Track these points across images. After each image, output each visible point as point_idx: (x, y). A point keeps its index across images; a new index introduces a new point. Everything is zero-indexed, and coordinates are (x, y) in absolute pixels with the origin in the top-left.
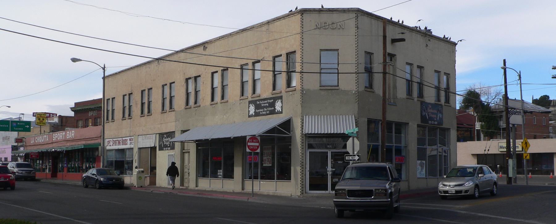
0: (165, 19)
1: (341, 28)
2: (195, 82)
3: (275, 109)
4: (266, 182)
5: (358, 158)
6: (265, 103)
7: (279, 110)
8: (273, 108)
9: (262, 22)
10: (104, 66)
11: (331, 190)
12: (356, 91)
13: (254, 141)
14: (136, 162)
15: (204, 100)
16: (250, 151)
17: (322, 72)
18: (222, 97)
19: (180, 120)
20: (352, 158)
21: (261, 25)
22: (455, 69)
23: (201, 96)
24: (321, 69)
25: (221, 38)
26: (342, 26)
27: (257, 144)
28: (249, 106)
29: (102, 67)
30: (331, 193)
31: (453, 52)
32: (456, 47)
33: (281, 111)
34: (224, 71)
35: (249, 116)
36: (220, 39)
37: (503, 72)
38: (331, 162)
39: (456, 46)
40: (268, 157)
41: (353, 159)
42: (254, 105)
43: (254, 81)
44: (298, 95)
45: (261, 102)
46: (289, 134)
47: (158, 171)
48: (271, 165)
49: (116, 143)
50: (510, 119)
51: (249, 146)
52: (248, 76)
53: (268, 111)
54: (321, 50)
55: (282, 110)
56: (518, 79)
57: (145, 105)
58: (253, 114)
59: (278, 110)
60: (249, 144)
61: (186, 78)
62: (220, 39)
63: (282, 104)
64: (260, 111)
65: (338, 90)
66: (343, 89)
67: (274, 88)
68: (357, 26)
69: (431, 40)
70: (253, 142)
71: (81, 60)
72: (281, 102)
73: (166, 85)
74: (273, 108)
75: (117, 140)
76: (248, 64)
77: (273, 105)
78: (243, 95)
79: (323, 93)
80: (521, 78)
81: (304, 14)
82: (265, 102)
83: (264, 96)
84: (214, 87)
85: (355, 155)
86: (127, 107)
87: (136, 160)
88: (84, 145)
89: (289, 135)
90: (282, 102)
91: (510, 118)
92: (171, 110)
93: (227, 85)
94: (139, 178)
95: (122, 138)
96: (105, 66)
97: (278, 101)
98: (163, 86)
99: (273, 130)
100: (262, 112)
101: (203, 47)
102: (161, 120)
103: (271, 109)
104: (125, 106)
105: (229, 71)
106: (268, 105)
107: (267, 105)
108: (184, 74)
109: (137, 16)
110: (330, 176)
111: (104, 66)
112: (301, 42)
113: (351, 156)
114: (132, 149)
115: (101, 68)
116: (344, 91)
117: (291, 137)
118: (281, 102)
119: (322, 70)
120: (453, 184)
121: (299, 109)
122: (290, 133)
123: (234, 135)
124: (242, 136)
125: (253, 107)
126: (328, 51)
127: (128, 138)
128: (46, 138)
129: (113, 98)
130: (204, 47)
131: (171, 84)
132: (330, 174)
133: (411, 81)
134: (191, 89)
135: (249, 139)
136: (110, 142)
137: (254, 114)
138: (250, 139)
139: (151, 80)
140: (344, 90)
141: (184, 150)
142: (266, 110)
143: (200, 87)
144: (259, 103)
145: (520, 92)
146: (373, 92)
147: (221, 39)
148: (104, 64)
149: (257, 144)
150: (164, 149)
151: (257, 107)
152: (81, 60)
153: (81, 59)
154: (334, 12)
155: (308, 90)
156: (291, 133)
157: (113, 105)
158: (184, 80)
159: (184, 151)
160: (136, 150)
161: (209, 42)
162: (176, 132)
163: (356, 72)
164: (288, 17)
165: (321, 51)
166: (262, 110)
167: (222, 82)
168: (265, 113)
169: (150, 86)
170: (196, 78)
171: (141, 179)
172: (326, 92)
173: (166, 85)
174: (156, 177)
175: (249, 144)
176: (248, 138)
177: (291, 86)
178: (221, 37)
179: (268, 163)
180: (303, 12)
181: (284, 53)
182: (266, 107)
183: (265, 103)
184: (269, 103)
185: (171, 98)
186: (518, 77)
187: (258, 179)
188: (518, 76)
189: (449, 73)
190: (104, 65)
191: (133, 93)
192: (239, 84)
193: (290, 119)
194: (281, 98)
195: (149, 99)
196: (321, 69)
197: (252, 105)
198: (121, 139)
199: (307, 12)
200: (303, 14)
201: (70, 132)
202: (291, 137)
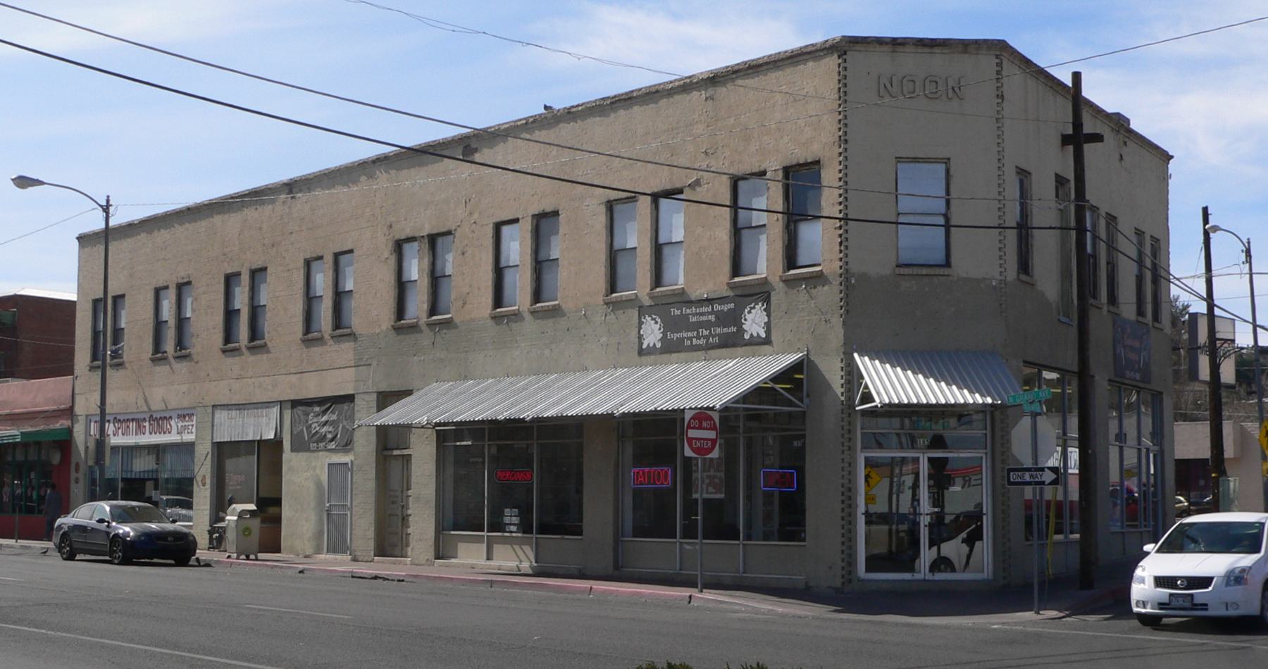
0: (528, 44)
1: (956, 91)
2: (429, 253)
3: (741, 331)
5: (1055, 476)
6: (702, 314)
7: (755, 335)
8: (733, 329)
9: (690, 77)
10: (108, 201)
12: (1001, 280)
13: (704, 424)
15: (464, 304)
16: (692, 454)
17: (900, 221)
19: (375, 363)
20: (1031, 476)
21: (688, 86)
22: (1168, 227)
23: (452, 292)
24: (899, 214)
26: (957, 90)
27: (711, 435)
28: (640, 323)
29: (101, 203)
30: (930, 579)
31: (1164, 178)
32: (1169, 166)
33: (763, 335)
34: (542, 218)
35: (641, 352)
37: (1202, 241)
38: (929, 487)
39: (1168, 163)
40: (712, 473)
41: (1036, 480)
42: (659, 321)
43: (658, 250)
44: (830, 295)
45: (689, 311)
46: (800, 404)
47: (287, 511)
48: (722, 496)
50: (1222, 366)
51: (690, 440)
52: (634, 236)
53: (714, 337)
54: (899, 159)
55: (768, 332)
56: (1244, 260)
58: (654, 344)
59: (752, 335)
60: (693, 433)
61: (396, 238)
63: (769, 315)
64: (685, 335)
67: (736, 270)
68: (1000, 93)
69: (1128, 143)
70: (700, 428)
71: (42, 183)
72: (765, 310)
73: (166, 288)
74: (733, 329)
77: (735, 318)
80: (1250, 256)
81: (848, 53)
82: (704, 309)
83: (697, 293)
86: (172, 323)
87: (204, 477)
89: (799, 407)
90: (768, 310)
91: (1220, 365)
94: (244, 532)
96: (111, 203)
97: (754, 308)
98: (308, 263)
99: (758, 393)
100: (690, 339)
102: (302, 361)
103: (725, 330)
105: (561, 217)
106: (713, 320)
107: (712, 318)
108: (391, 226)
109: (453, 31)
111: (108, 201)
112: (841, 133)
113: (1029, 470)
114: (189, 447)
115: (97, 206)
118: (765, 310)
119: (900, 215)
121: (836, 334)
122: (802, 403)
125: (658, 326)
126: (919, 162)
131: (337, 256)
132: (927, 523)
133: (1092, 256)
135: (691, 419)
136: (190, 427)
137: (659, 345)
138: (693, 418)
139: (264, 245)
142: (706, 333)
143: (450, 263)
144: (678, 312)
145: (1256, 293)
146: (1033, 285)
148: (108, 197)
149: (711, 435)
150: (313, 446)
151: (670, 325)
152: (42, 183)
153: (40, 179)
154: (936, 50)
156: (806, 400)
158: (390, 245)
160: (204, 451)
163: (1000, 224)
165: (898, 162)
166: (690, 334)
167: (536, 251)
168: (702, 341)
169: (260, 263)
170: (433, 239)
171: (250, 534)
172: (914, 282)
173: (166, 288)
174: (280, 528)
175: (693, 433)
176: (688, 416)
177: (313, 331)
178: (531, 120)
179: (711, 489)
180: (846, 47)
181: (774, 165)
182: (707, 325)
183: (702, 314)
184: (718, 315)
186: (1244, 254)
188: (1242, 251)
189: (1159, 238)
190: (106, 198)
191: (193, 282)
192: (602, 257)
193: (803, 360)
194: (766, 298)
196: (899, 214)
197: (653, 319)
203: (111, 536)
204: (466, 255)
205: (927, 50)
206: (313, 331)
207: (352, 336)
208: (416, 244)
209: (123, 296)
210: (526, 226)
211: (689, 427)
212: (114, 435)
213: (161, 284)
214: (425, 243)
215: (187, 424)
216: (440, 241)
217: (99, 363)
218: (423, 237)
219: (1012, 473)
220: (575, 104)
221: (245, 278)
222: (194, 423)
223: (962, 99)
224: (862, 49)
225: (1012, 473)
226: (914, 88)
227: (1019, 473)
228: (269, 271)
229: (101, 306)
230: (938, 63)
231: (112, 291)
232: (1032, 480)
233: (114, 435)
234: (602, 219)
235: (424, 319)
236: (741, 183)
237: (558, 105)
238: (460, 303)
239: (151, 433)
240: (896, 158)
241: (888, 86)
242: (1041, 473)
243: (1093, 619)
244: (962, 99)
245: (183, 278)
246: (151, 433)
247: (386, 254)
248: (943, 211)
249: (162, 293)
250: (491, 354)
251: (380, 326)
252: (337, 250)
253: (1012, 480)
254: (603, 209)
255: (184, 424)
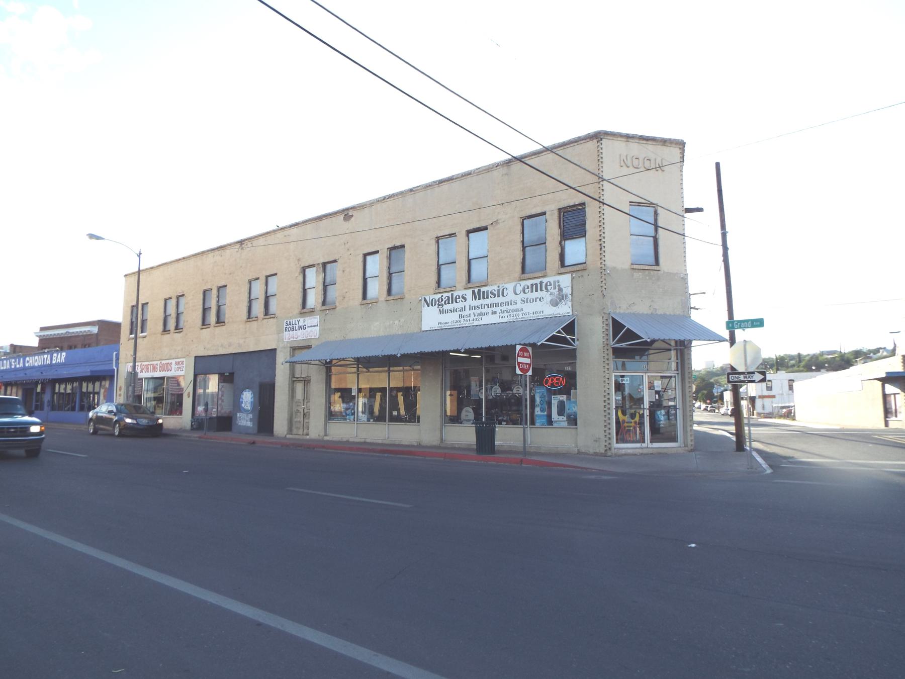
4: (500, 428)
5: (763, 377)
11: (651, 442)
14: (189, 397)
18: (388, 291)
25: (388, 199)
36: (384, 199)
41: (749, 379)
43: (267, 299)
49: (148, 368)
57: (147, 322)
60: (520, 360)
62: (384, 199)
65: (659, 272)
66: (666, 271)
70: (523, 356)
73: (170, 298)
75: (151, 365)
76: (455, 234)
78: (439, 287)
79: (637, 275)
81: (603, 139)
84: (366, 277)
85: (753, 373)
86: (174, 315)
88: (91, 372)
92: (266, 317)
93: (404, 271)
95: (140, 362)
98: (166, 300)
101: (343, 215)
104: (167, 314)
110: (648, 417)
116: (669, 274)
117: (575, 350)
120: (196, 435)
123: (464, 345)
124: (432, 352)
127: (173, 361)
128: (47, 358)
129: (221, 288)
130: (345, 215)
134: (172, 310)
139: (225, 274)
140: (668, 273)
141: (295, 377)
147: (386, 200)
154: (649, 142)
155: (615, 268)
157: (143, 314)
158: (299, 270)
159: (294, 379)
161: (358, 207)
162: (278, 352)
164: (562, 148)
173: (170, 298)
175: (520, 360)
177: (269, 314)
181: (384, 248)
185: (178, 316)
187: (386, 421)
195: (218, 301)
198: (159, 362)
199: (609, 138)
200: (601, 139)
201: (57, 356)
202: (575, 350)
203: (114, 420)
204: (345, 272)
205: (645, 142)
206: (269, 314)
207: (274, 316)
208: (314, 269)
209: (147, 303)
210: (384, 254)
211: (518, 356)
212: (141, 372)
213: (168, 296)
214: (320, 268)
215: (180, 366)
216: (328, 266)
217: (133, 336)
218: (319, 264)
219: (730, 376)
220: (415, 186)
221: (215, 292)
222: (184, 365)
223: (663, 171)
224: (611, 138)
225: (730, 376)
226: (639, 163)
227: (736, 376)
228: (228, 287)
229: (135, 308)
230: (650, 150)
231: (141, 302)
232: (745, 379)
233: (141, 372)
234: (434, 247)
235: (319, 307)
236: (369, 258)
237: (281, 226)
238: (342, 298)
239: (160, 371)
240: (630, 202)
241: (625, 160)
242: (752, 375)
243: (196, 435)
244: (663, 171)
245: (180, 293)
246: (160, 371)
247: (297, 274)
248: (653, 235)
249: (168, 301)
250: (361, 324)
251: (292, 312)
252: (219, 285)
253: (731, 380)
254: (434, 242)
255: (179, 366)
